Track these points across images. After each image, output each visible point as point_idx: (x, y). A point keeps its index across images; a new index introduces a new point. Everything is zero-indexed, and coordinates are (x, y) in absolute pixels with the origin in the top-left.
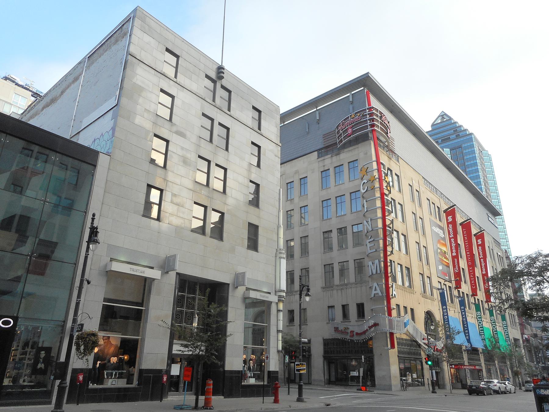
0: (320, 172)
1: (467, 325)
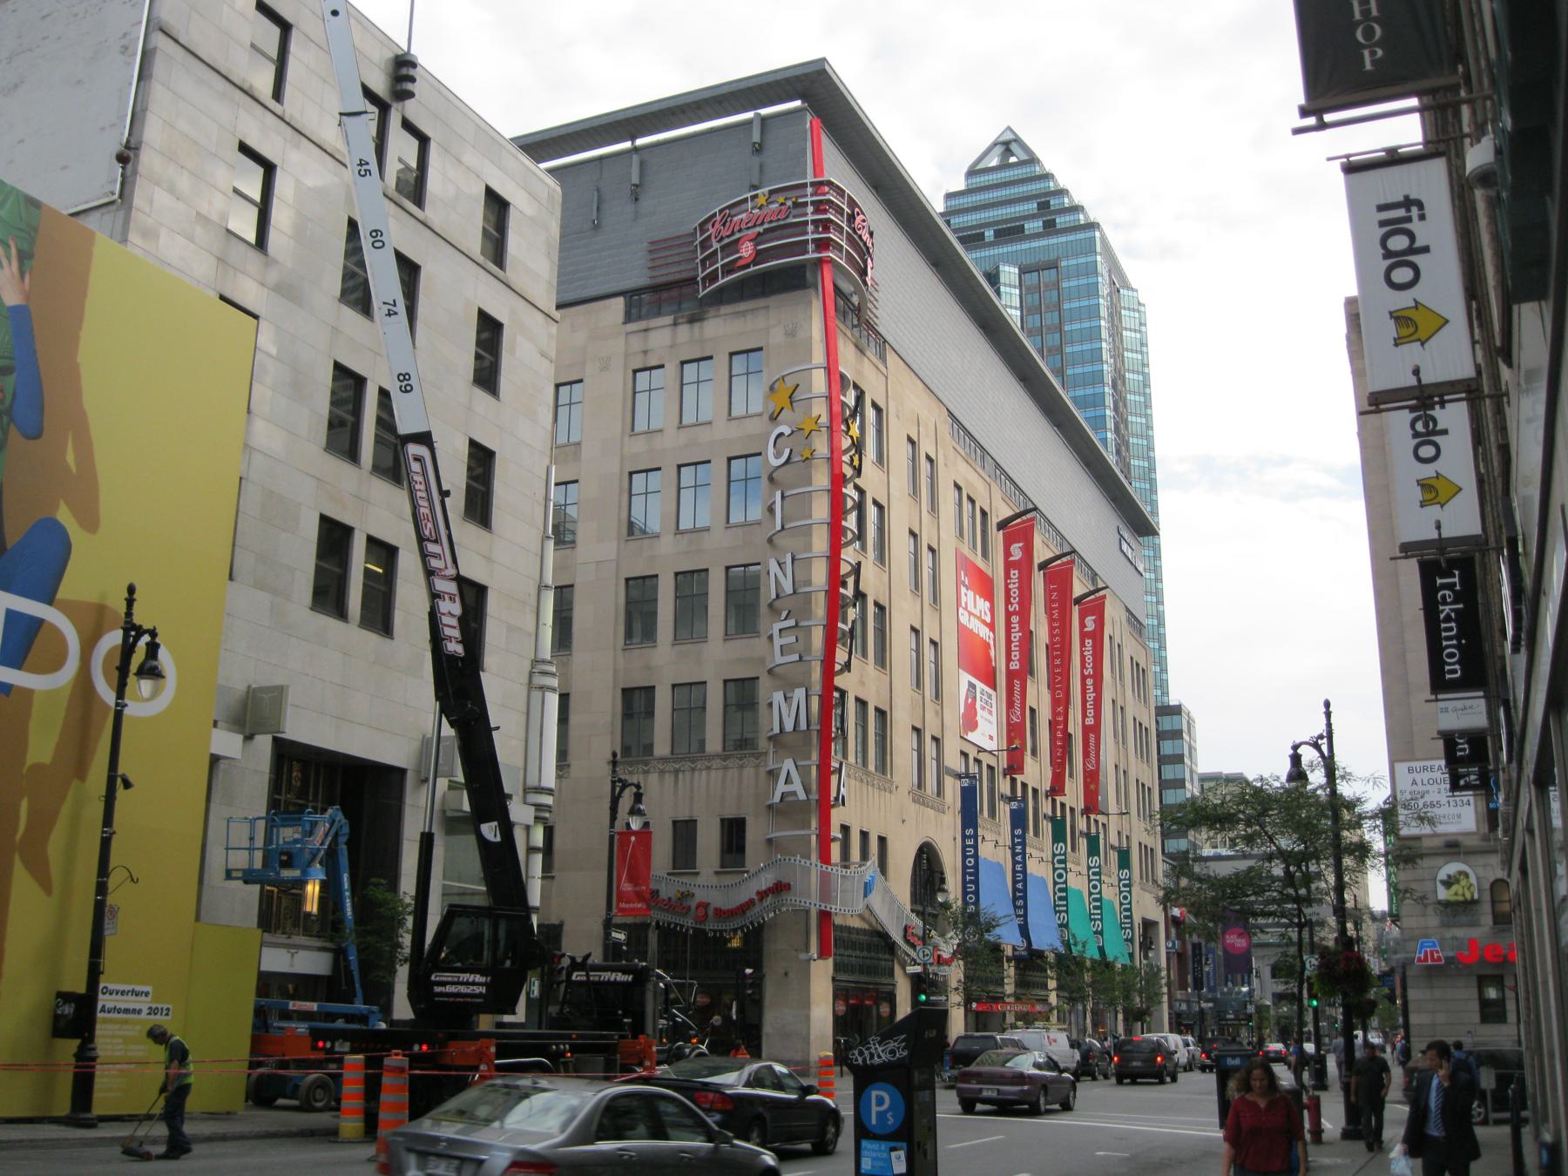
0: (631, 373)
1: (1025, 886)
